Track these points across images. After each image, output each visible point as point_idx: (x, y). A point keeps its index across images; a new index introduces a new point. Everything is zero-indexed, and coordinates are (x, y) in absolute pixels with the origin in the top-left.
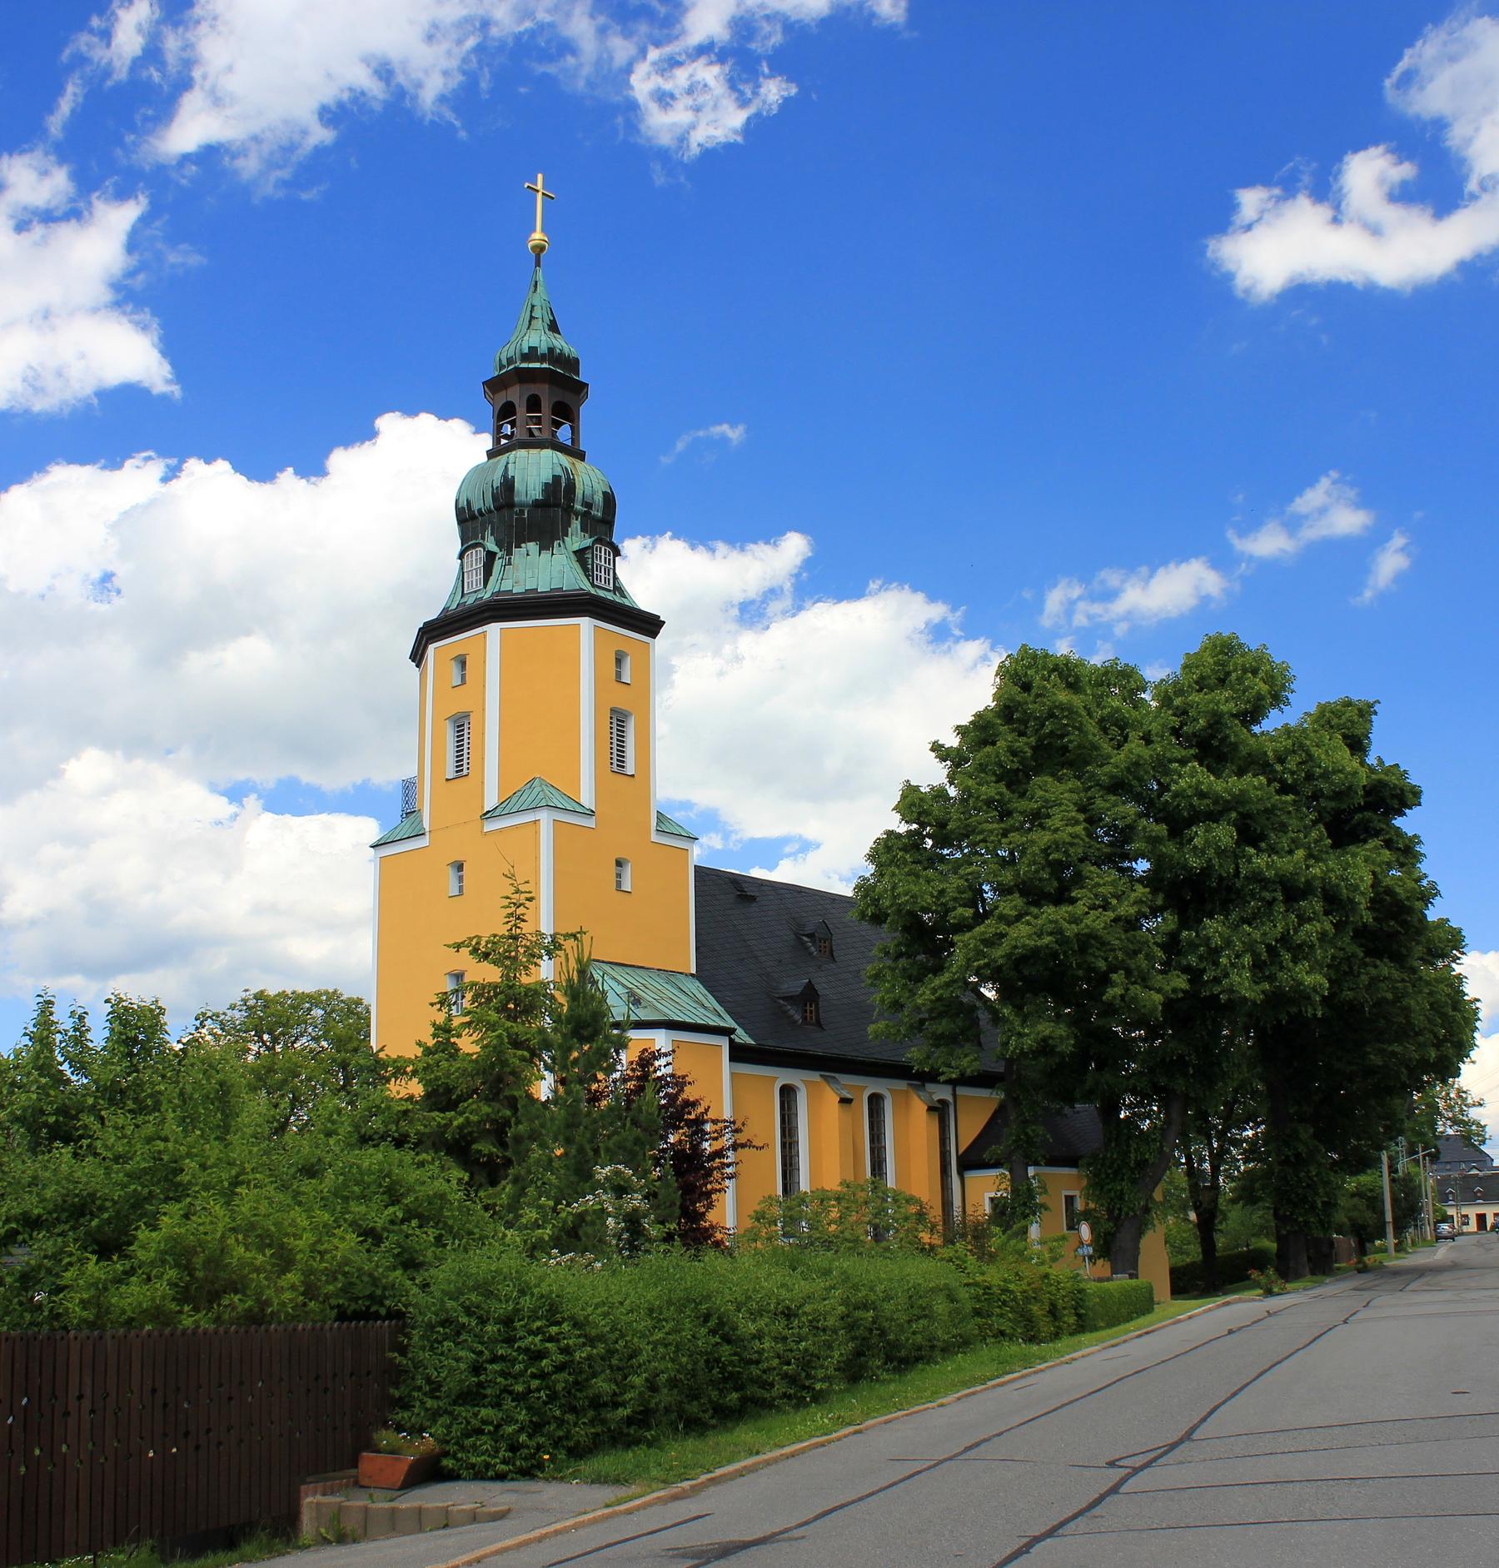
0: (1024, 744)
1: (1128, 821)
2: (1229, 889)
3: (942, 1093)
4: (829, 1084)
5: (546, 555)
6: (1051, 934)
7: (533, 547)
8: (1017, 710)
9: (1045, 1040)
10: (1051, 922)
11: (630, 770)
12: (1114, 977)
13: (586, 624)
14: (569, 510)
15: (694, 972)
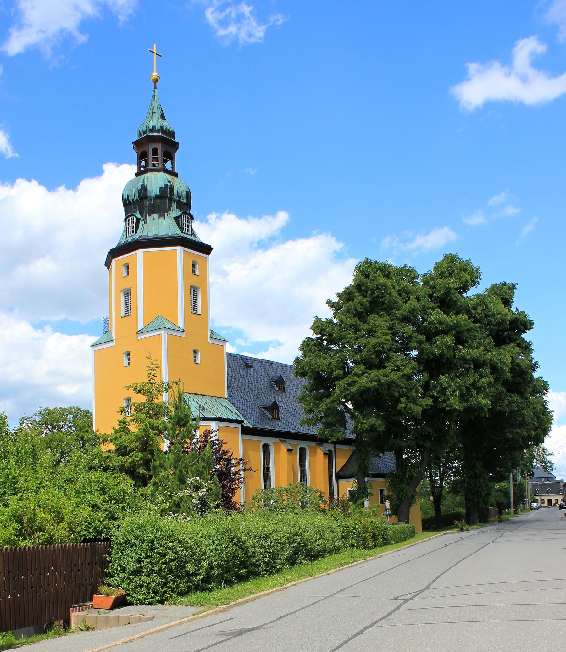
0: (366, 301)
1: (409, 334)
2: (451, 363)
3: (330, 447)
4: (282, 442)
5: (162, 219)
7: (156, 215)
9: (372, 425)
10: (376, 376)
11: (199, 312)
12: (402, 399)
13: (179, 249)
14: (171, 200)
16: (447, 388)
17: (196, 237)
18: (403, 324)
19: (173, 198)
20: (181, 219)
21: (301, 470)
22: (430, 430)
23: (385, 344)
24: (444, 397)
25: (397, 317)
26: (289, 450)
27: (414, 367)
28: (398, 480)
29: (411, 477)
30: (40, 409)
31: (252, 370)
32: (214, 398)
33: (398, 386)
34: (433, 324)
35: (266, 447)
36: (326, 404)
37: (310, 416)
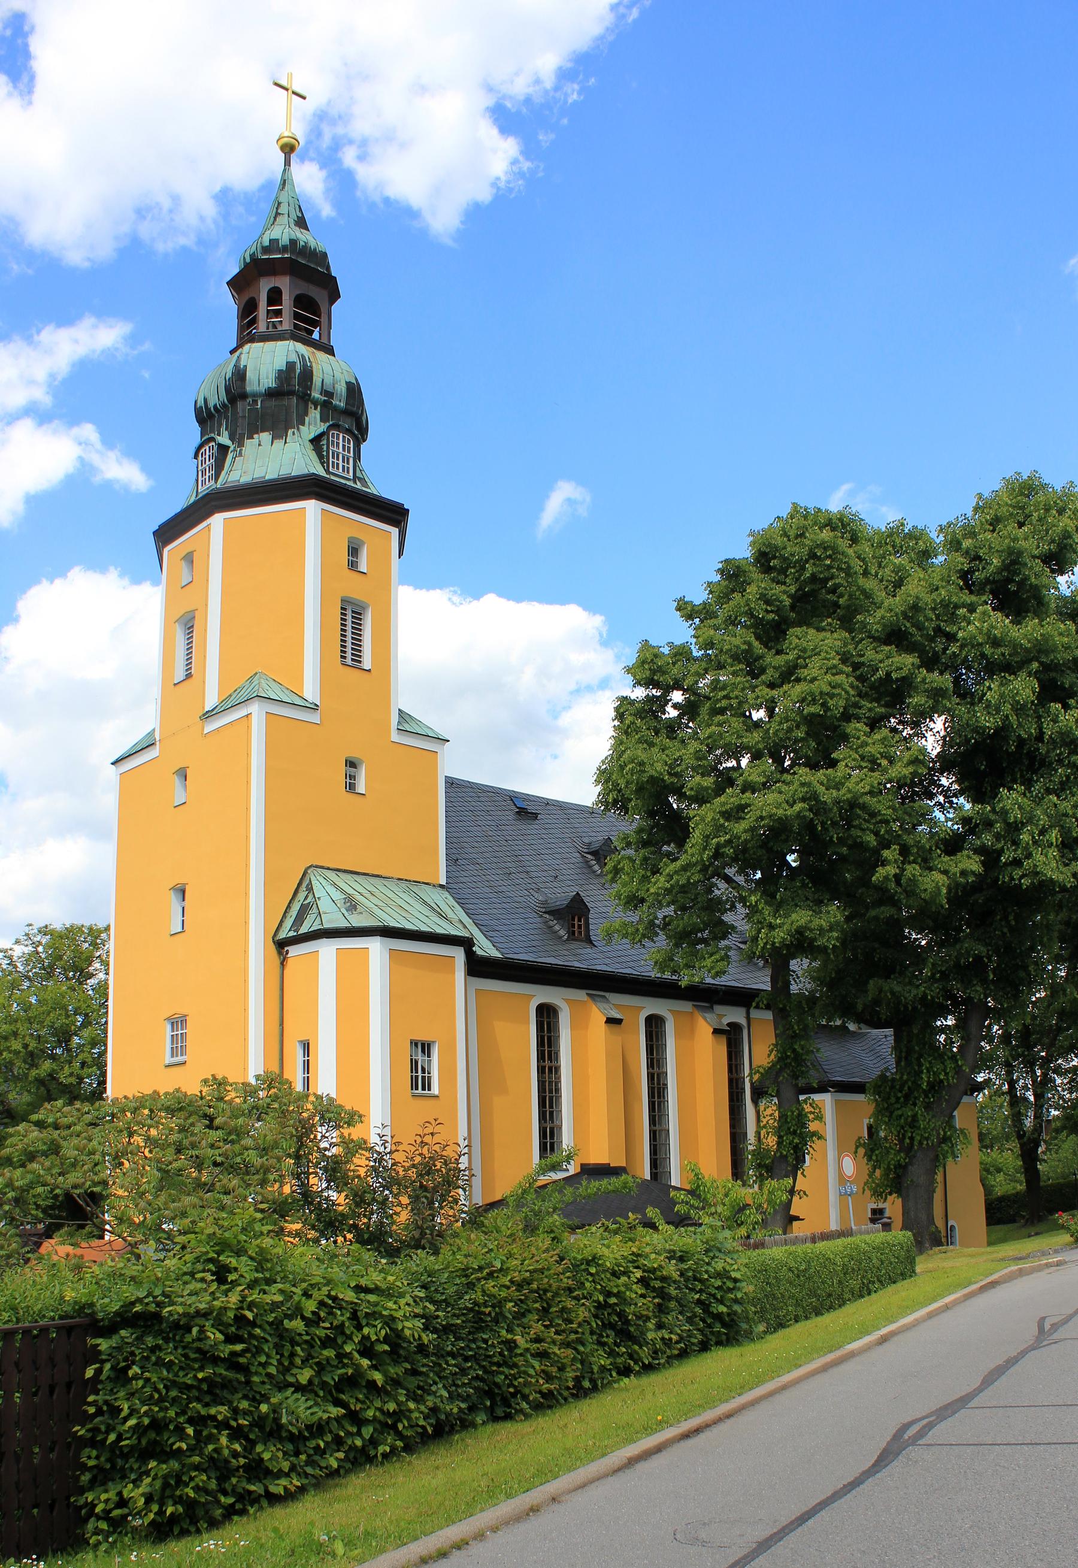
0: (783, 593)
1: (904, 673)
2: (1032, 756)
3: (735, 1015)
4: (594, 1000)
5: (279, 443)
6: (803, 800)
7: (265, 437)
8: (774, 557)
9: (800, 931)
10: (803, 785)
11: (367, 663)
12: (886, 853)
13: (312, 508)
14: (305, 398)
15: (443, 882)
16: (1022, 823)
17: (368, 487)
18: (887, 648)
19: (310, 395)
20: (324, 442)
21: (651, 1077)
22: (980, 949)
23: (832, 696)
24: (1015, 850)
25: (870, 632)
26: (610, 1021)
27: (917, 758)
28: (899, 1095)
29: (936, 1087)
30: (27, 930)
31: (532, 828)
32: (404, 885)
33: (873, 815)
34: (973, 646)
35: (547, 1015)
36: (668, 875)
37: (633, 917)
